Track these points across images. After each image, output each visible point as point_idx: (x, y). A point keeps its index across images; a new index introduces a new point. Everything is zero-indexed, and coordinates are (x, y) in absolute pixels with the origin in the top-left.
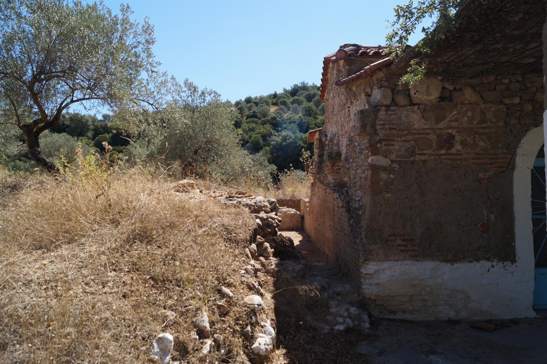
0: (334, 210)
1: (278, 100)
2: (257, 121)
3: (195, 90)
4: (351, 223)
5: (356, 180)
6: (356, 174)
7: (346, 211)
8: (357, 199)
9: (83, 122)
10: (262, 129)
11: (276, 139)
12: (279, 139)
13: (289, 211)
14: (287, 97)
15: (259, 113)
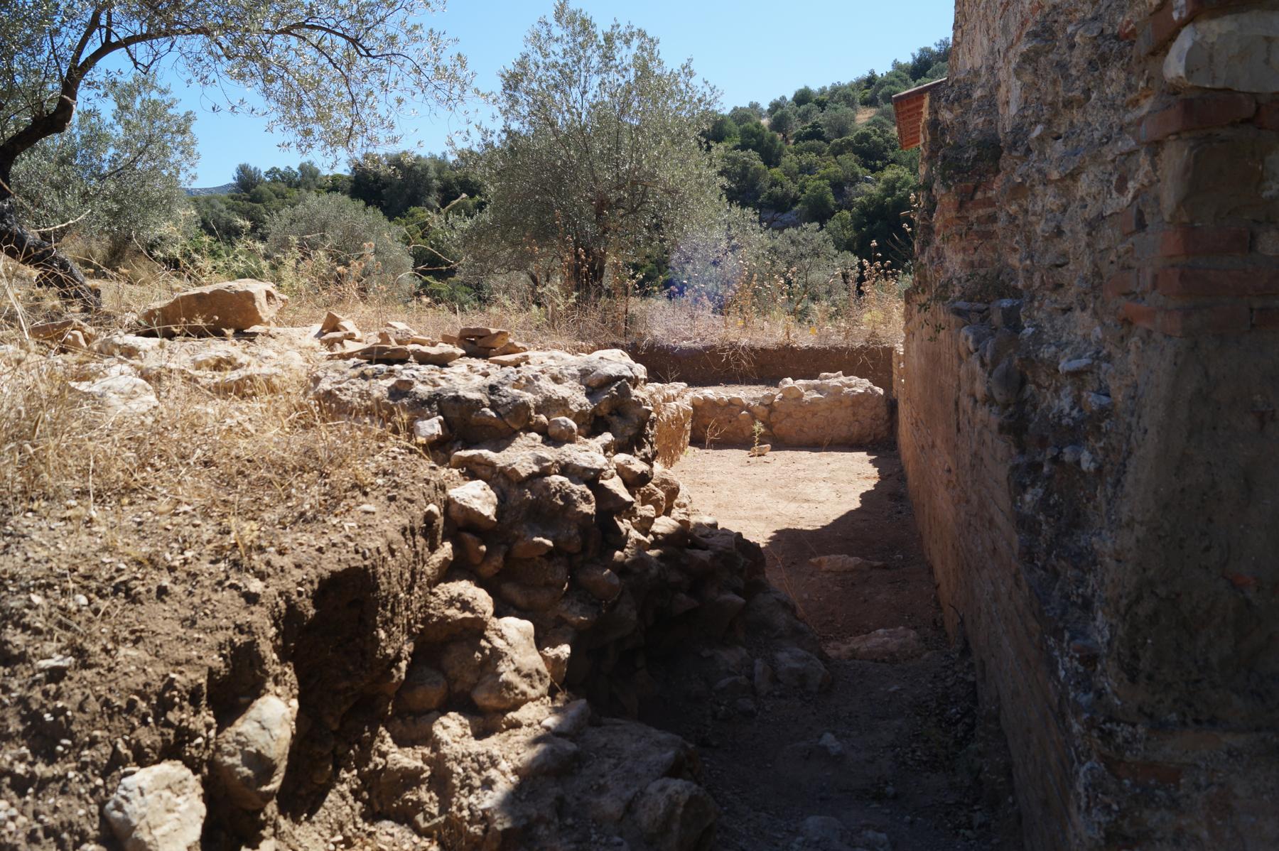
0: (957, 404)
1: (876, 92)
2: (821, 147)
3: (586, 26)
4: (1027, 510)
5: (1066, 244)
6: (1064, 209)
7: (1001, 429)
8: (1064, 366)
9: (417, 172)
10: (833, 168)
11: (870, 188)
12: (875, 190)
13: (850, 386)
14: (902, 81)
15: (826, 126)
